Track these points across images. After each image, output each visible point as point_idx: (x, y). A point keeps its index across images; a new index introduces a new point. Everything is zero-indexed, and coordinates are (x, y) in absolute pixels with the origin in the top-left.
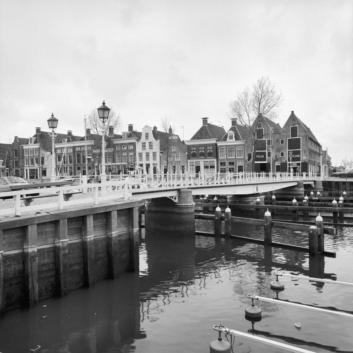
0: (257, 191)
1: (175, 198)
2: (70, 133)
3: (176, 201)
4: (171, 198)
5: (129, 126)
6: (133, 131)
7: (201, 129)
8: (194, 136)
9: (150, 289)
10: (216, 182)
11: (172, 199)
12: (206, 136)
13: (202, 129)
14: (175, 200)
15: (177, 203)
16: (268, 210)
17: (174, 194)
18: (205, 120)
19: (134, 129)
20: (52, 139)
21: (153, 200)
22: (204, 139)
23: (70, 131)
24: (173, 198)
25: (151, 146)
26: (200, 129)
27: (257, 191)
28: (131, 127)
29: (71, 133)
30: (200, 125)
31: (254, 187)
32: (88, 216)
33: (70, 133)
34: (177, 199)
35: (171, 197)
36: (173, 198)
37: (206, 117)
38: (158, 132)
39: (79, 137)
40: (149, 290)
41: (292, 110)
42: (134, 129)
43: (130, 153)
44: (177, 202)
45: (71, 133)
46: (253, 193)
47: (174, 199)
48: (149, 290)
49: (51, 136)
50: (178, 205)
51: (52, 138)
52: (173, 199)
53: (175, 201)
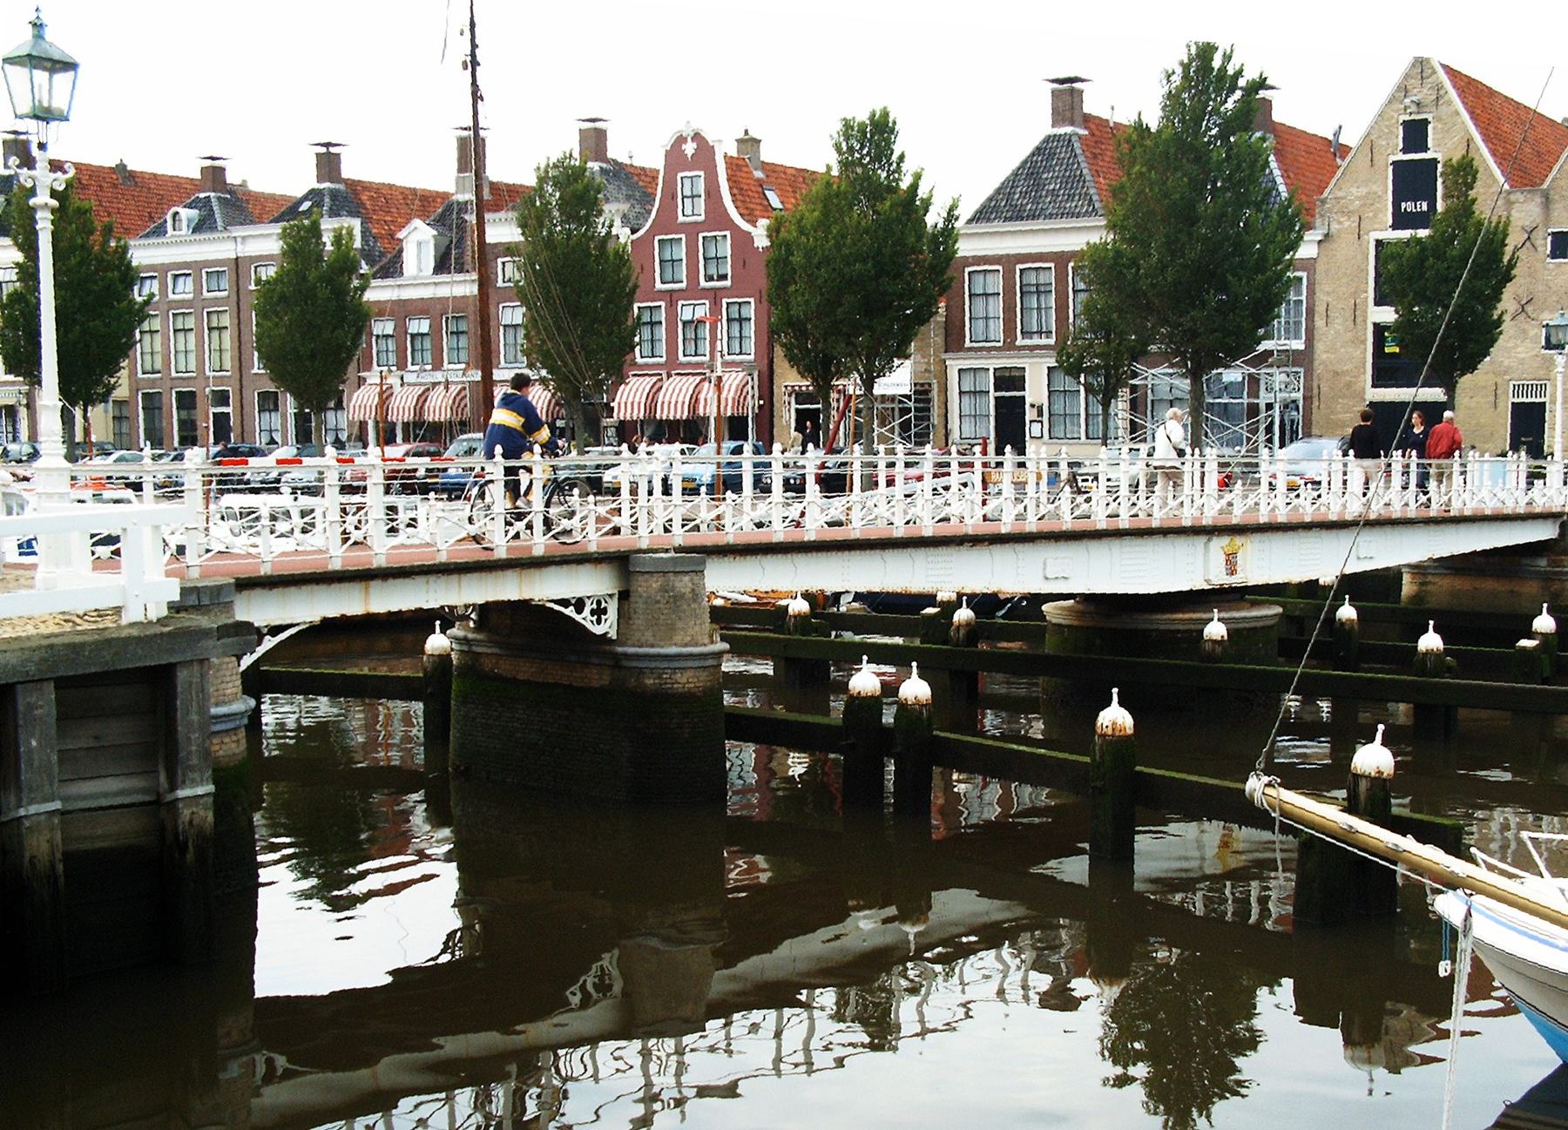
0: (1232, 572)
1: (599, 612)
2: (214, 175)
3: (607, 627)
4: (570, 611)
5: (1053, 92)
6: (607, 161)
7: (1038, 150)
8: (990, 199)
9: (1328, 791)
10: (967, 512)
11: (578, 618)
12: (1071, 197)
13: (1045, 151)
14: (599, 622)
15: (611, 641)
16: (1545, 610)
17: (593, 584)
18: (1067, 96)
19: (349, 171)
20: (32, 202)
21: (487, 611)
22: (1051, 216)
23: (593, 120)
24: (579, 611)
25: (673, 261)
26: (1033, 154)
27: (1232, 572)
28: (328, 163)
29: (222, 170)
30: (1037, 125)
31: (1206, 544)
32: (178, 666)
33: (214, 175)
34: (612, 614)
35: (565, 603)
36: (579, 611)
37: (1072, 75)
38: (765, 166)
39: (273, 198)
40: (1325, 794)
41: (49, 146)
42: (349, 171)
43: (380, 325)
44: (613, 634)
45: (222, 170)
46: (1199, 584)
47: (593, 612)
48: (1325, 794)
49: (29, 184)
50: (627, 656)
51: (32, 192)
52: (585, 618)
53: (598, 630)
